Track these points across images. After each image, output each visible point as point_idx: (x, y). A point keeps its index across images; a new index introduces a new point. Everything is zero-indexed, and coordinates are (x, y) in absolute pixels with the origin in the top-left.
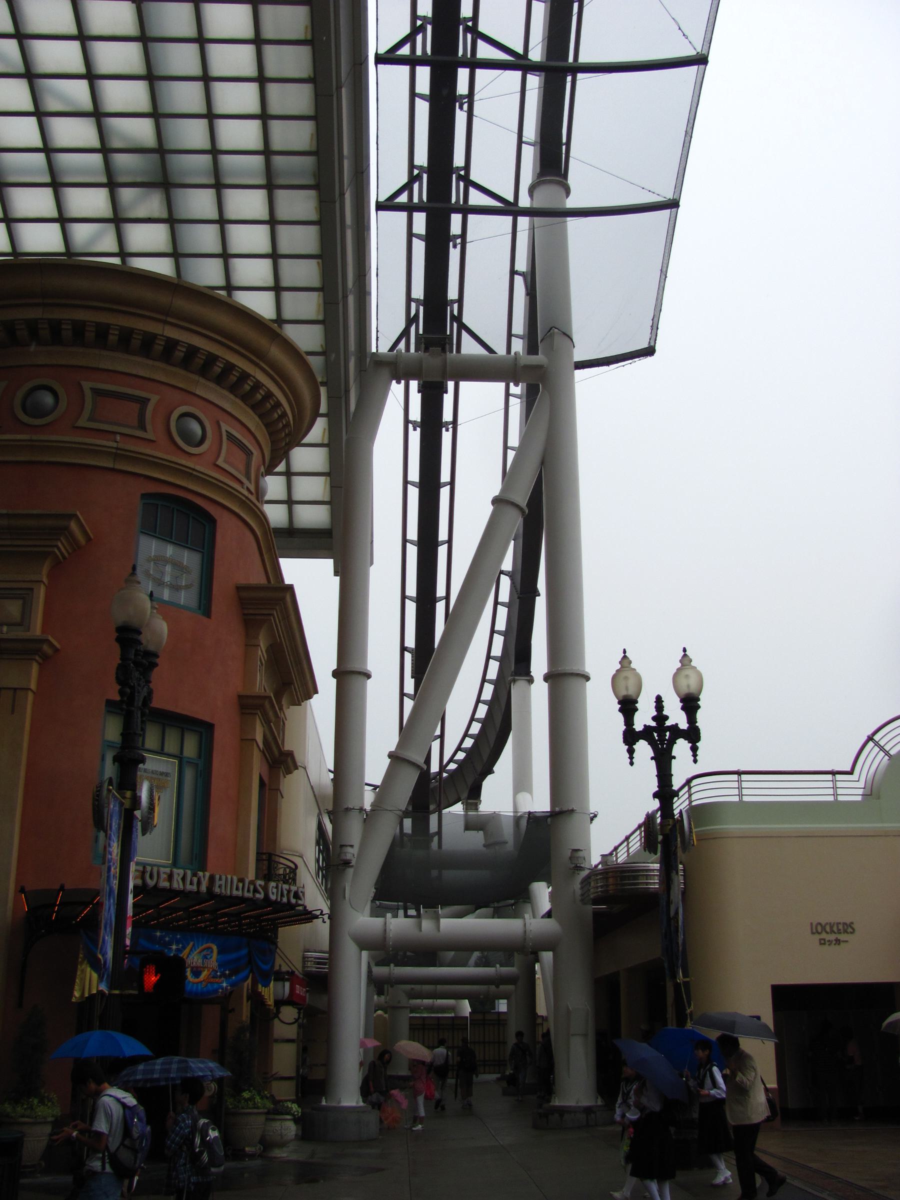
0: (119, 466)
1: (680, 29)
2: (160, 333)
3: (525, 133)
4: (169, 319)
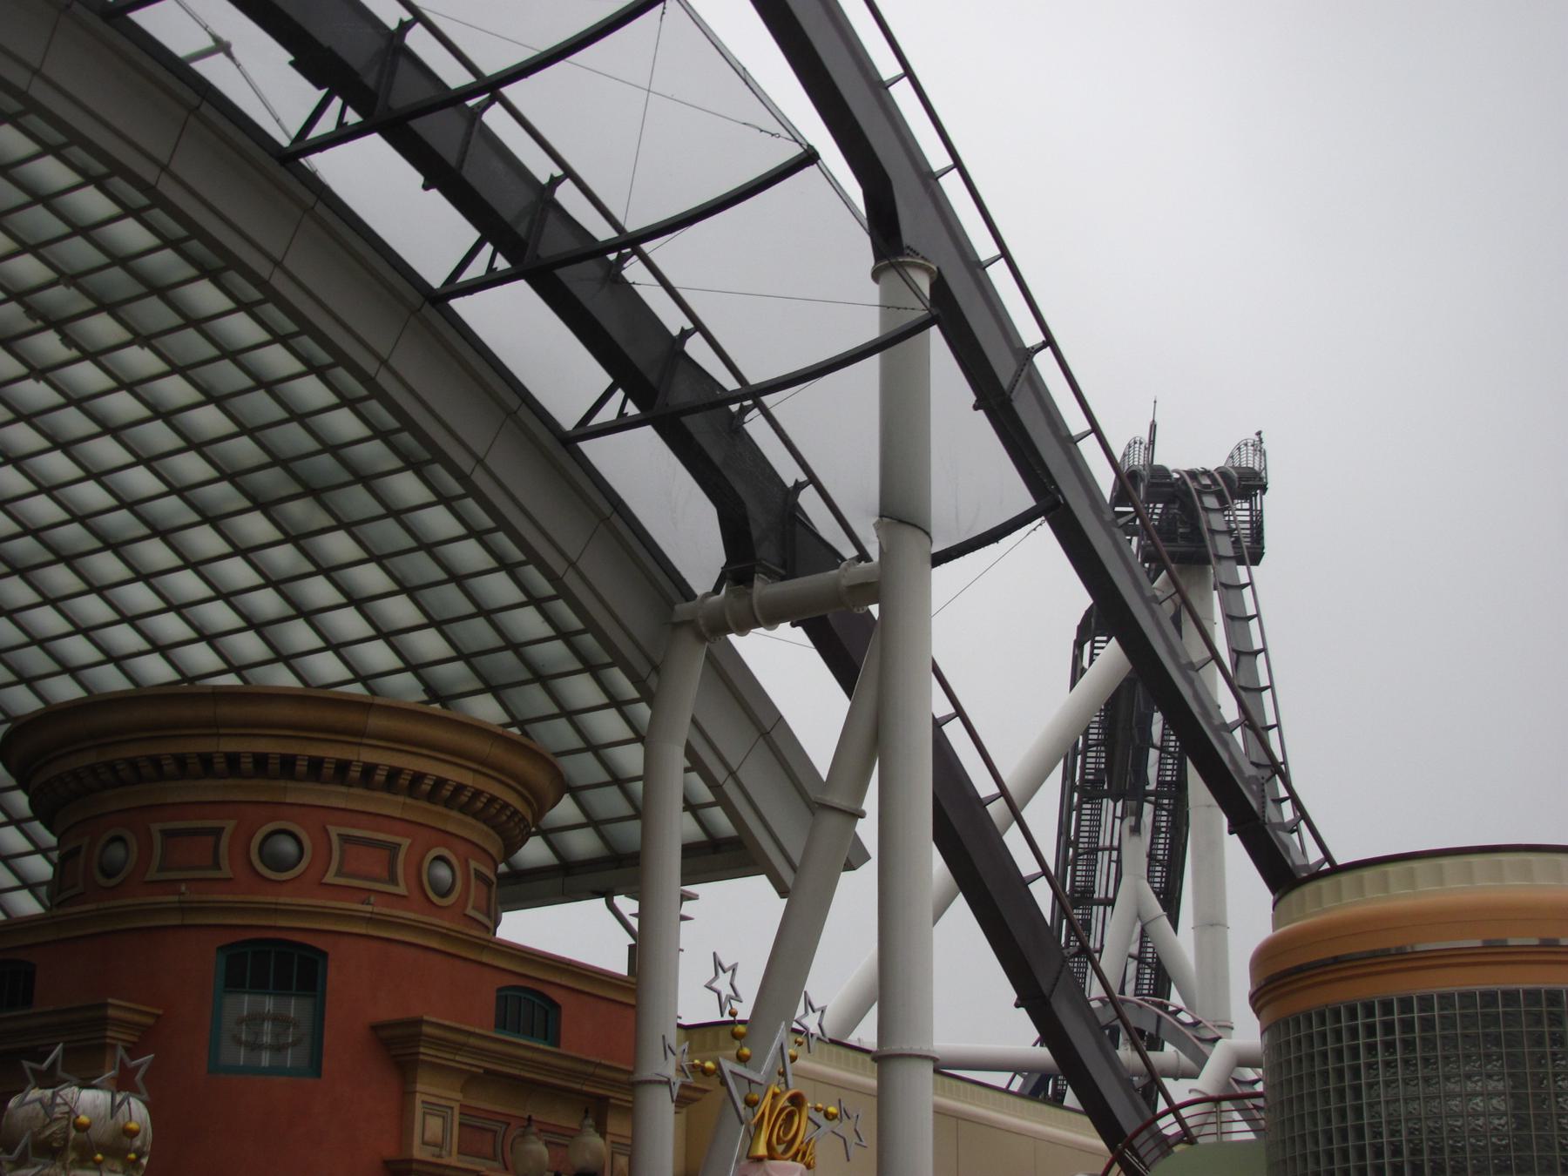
0: (189, 921)
1: (762, 131)
2: (356, 758)
3: (762, 419)
4: (222, 731)
